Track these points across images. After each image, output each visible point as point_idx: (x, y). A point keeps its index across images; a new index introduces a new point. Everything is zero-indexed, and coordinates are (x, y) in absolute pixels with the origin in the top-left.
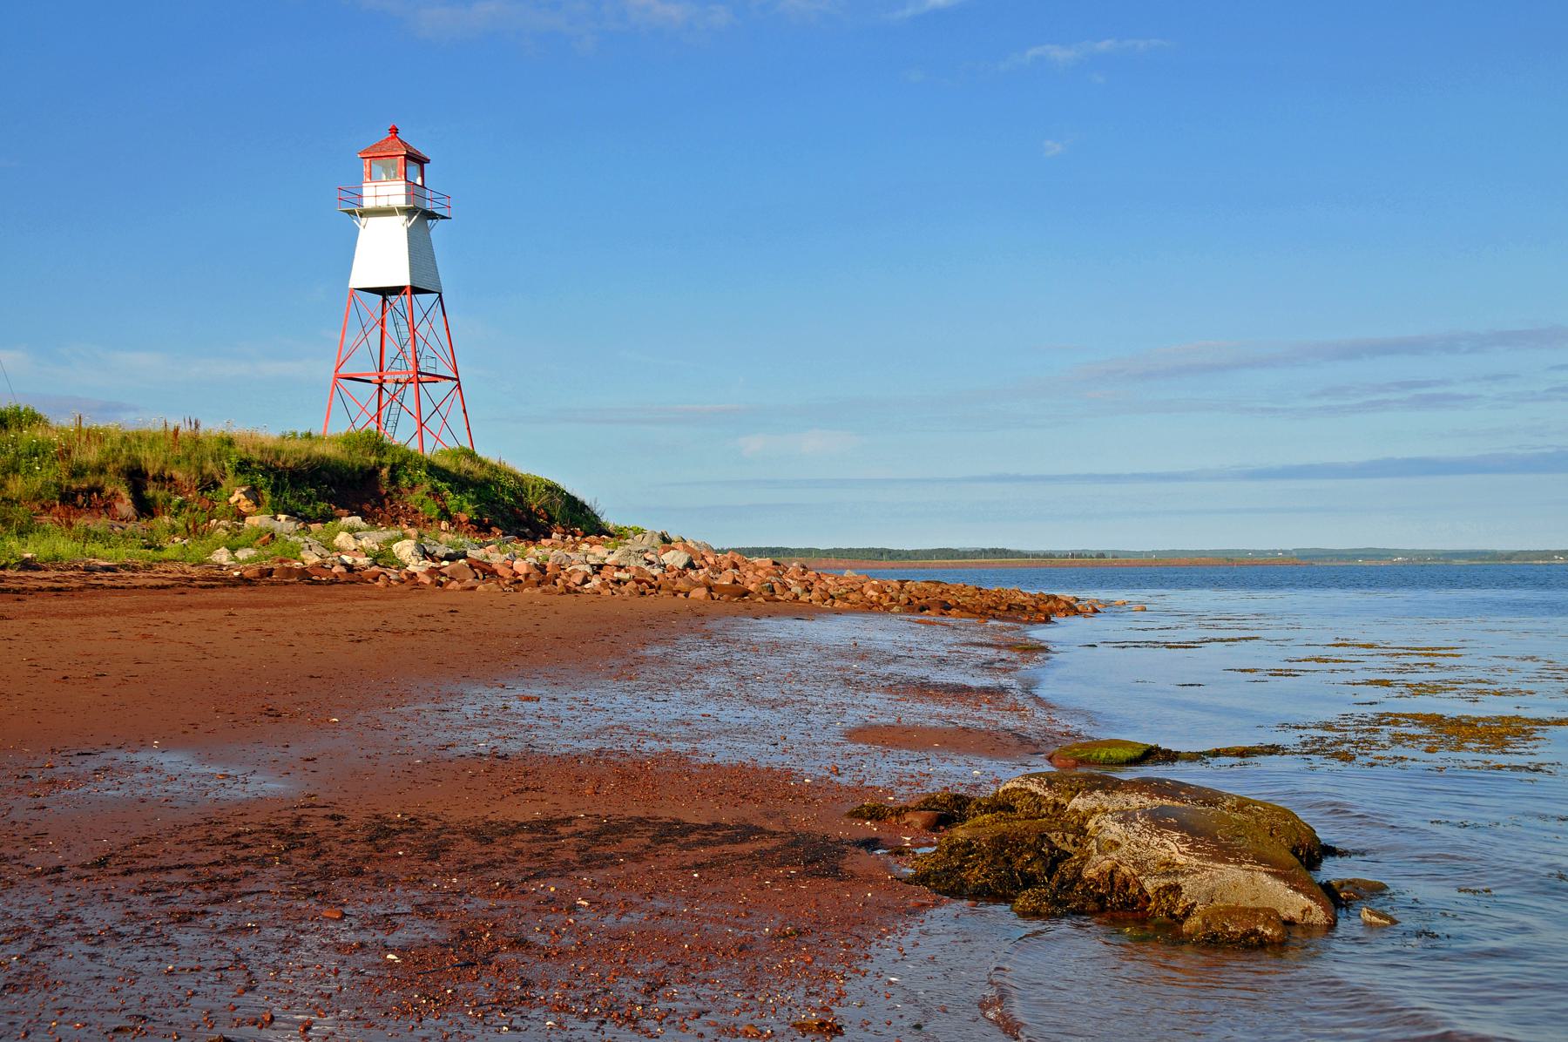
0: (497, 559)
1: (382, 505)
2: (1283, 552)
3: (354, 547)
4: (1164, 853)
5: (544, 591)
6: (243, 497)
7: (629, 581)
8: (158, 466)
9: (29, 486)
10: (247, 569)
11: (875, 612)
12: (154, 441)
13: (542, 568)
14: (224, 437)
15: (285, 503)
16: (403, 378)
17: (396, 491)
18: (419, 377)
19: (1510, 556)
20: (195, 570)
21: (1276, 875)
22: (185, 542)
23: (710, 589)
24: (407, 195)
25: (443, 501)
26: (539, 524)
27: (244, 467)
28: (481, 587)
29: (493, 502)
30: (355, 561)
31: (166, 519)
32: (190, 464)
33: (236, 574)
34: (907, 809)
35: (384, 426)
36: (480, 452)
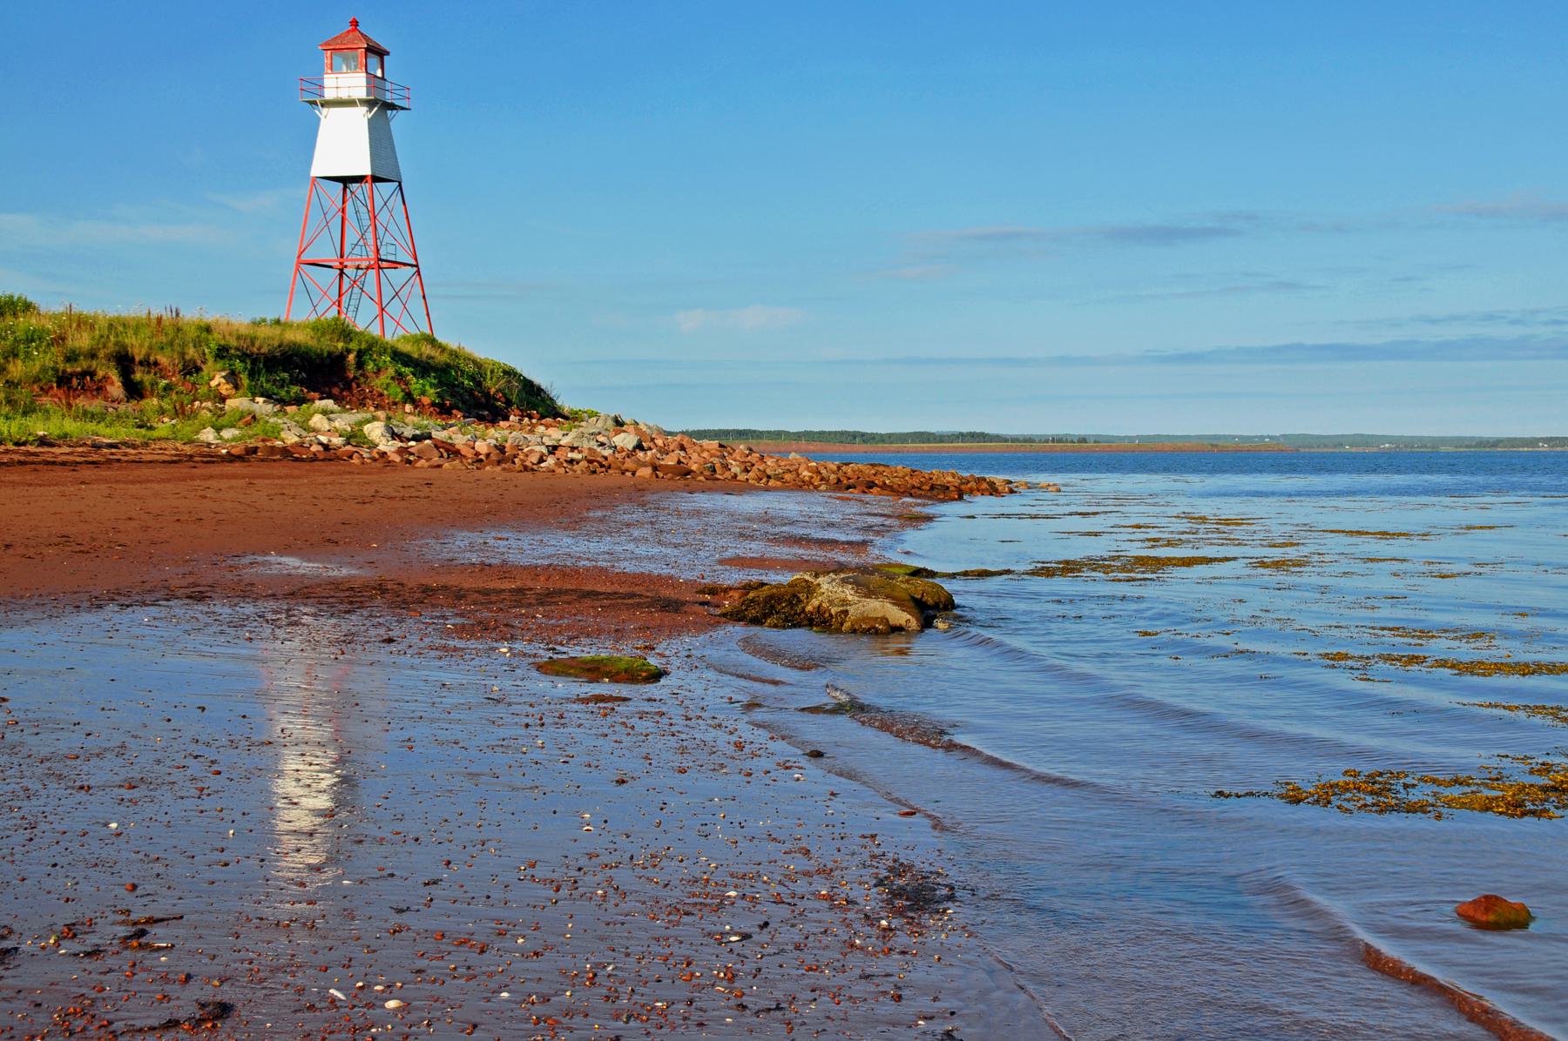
0: (460, 440)
1: (349, 389)
2: (1271, 438)
3: (328, 428)
4: (843, 595)
5: (504, 469)
6: (223, 381)
7: (581, 460)
8: (144, 351)
9: (29, 370)
10: (233, 447)
11: (806, 491)
12: (138, 327)
13: (501, 449)
14: (202, 324)
15: (262, 386)
16: (364, 264)
17: (363, 375)
18: (380, 264)
19: (1496, 443)
20: (187, 448)
21: (894, 604)
22: (174, 422)
23: (655, 468)
24: (368, 87)
25: (406, 385)
26: (497, 407)
27: (222, 353)
28: (446, 465)
29: (454, 386)
30: (330, 441)
31: (155, 401)
32: (173, 350)
33: (224, 451)
34: (731, 589)
35: (345, 311)
36: (441, 338)
